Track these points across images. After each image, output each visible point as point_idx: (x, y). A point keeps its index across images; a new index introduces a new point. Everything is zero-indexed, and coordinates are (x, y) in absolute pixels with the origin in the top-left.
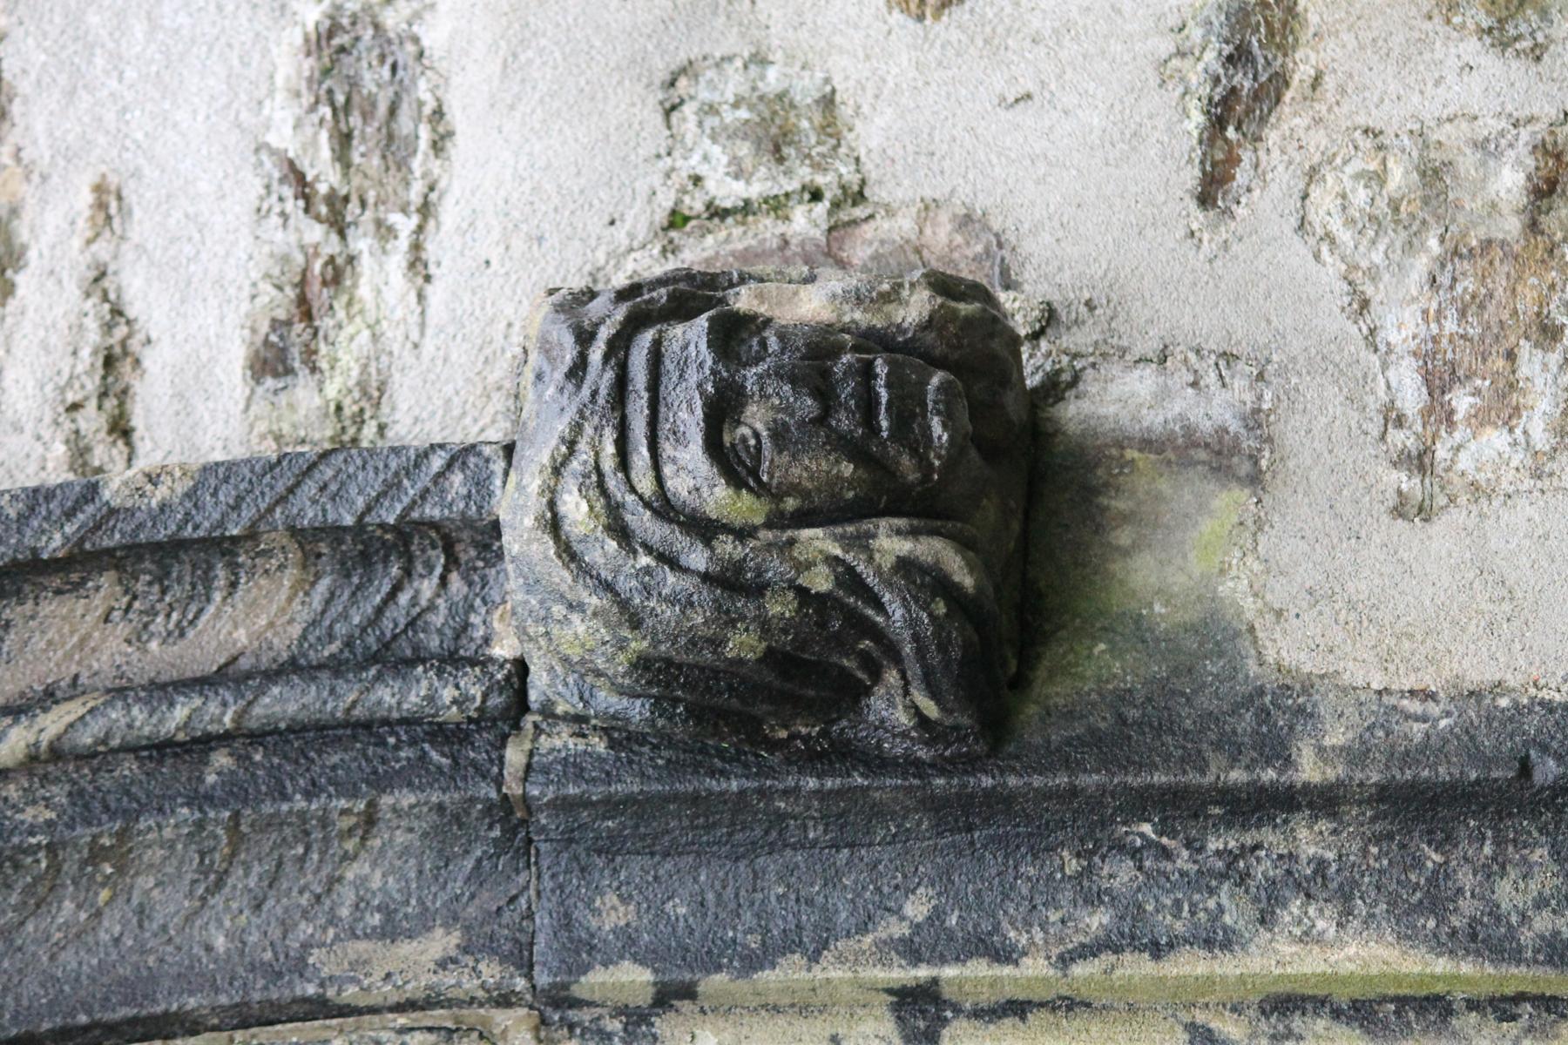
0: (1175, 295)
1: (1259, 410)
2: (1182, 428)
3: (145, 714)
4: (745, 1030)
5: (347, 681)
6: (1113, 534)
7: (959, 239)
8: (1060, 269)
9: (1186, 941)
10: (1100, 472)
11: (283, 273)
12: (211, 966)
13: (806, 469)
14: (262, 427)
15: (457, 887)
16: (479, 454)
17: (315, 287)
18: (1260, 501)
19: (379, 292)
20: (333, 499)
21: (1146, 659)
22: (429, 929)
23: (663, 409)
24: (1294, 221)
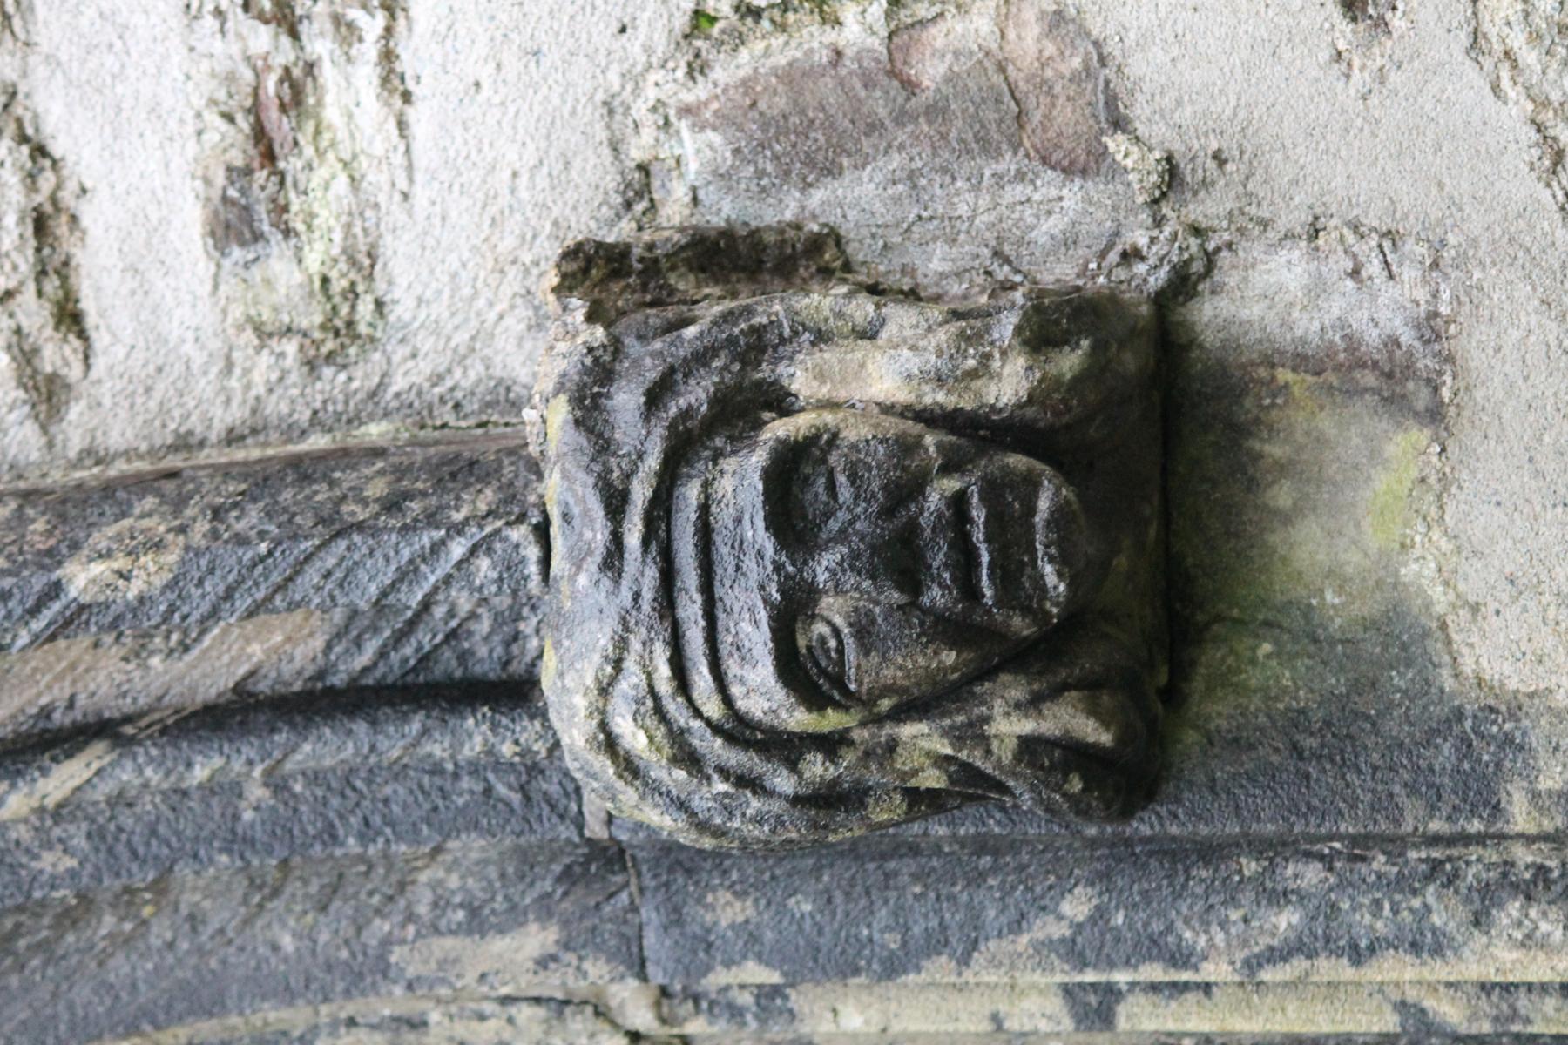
0: (1322, 146)
1: (1436, 314)
2: (1343, 337)
3: (161, 774)
4: (893, 1006)
5: (388, 737)
6: (1270, 493)
7: (1050, 49)
8: (1179, 103)
9: (1389, 945)
10: (1248, 403)
11: (231, 96)
12: (282, 967)
13: (901, 668)
14: (237, 312)
15: (547, 885)
16: (506, 539)
17: (272, 115)
18: (1443, 450)
19: (350, 116)
20: (341, 585)
21: (1320, 668)
22: (522, 924)
23: (721, 616)
24: (1464, 38)
